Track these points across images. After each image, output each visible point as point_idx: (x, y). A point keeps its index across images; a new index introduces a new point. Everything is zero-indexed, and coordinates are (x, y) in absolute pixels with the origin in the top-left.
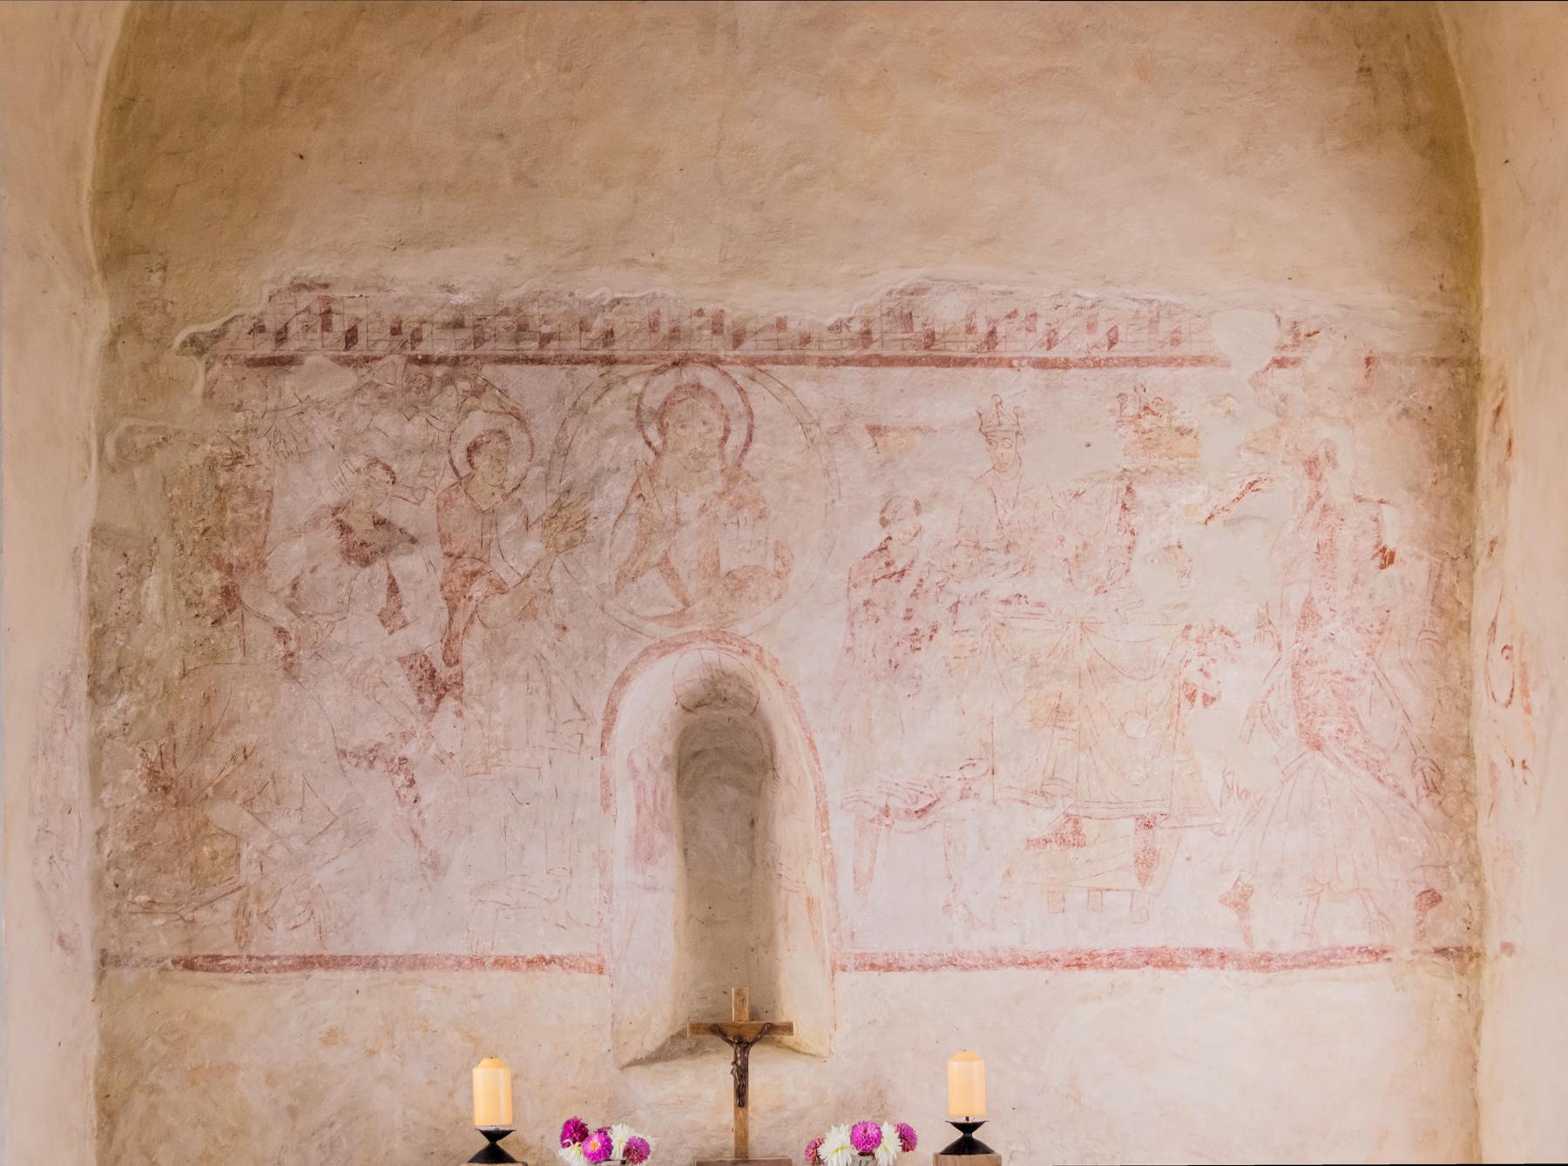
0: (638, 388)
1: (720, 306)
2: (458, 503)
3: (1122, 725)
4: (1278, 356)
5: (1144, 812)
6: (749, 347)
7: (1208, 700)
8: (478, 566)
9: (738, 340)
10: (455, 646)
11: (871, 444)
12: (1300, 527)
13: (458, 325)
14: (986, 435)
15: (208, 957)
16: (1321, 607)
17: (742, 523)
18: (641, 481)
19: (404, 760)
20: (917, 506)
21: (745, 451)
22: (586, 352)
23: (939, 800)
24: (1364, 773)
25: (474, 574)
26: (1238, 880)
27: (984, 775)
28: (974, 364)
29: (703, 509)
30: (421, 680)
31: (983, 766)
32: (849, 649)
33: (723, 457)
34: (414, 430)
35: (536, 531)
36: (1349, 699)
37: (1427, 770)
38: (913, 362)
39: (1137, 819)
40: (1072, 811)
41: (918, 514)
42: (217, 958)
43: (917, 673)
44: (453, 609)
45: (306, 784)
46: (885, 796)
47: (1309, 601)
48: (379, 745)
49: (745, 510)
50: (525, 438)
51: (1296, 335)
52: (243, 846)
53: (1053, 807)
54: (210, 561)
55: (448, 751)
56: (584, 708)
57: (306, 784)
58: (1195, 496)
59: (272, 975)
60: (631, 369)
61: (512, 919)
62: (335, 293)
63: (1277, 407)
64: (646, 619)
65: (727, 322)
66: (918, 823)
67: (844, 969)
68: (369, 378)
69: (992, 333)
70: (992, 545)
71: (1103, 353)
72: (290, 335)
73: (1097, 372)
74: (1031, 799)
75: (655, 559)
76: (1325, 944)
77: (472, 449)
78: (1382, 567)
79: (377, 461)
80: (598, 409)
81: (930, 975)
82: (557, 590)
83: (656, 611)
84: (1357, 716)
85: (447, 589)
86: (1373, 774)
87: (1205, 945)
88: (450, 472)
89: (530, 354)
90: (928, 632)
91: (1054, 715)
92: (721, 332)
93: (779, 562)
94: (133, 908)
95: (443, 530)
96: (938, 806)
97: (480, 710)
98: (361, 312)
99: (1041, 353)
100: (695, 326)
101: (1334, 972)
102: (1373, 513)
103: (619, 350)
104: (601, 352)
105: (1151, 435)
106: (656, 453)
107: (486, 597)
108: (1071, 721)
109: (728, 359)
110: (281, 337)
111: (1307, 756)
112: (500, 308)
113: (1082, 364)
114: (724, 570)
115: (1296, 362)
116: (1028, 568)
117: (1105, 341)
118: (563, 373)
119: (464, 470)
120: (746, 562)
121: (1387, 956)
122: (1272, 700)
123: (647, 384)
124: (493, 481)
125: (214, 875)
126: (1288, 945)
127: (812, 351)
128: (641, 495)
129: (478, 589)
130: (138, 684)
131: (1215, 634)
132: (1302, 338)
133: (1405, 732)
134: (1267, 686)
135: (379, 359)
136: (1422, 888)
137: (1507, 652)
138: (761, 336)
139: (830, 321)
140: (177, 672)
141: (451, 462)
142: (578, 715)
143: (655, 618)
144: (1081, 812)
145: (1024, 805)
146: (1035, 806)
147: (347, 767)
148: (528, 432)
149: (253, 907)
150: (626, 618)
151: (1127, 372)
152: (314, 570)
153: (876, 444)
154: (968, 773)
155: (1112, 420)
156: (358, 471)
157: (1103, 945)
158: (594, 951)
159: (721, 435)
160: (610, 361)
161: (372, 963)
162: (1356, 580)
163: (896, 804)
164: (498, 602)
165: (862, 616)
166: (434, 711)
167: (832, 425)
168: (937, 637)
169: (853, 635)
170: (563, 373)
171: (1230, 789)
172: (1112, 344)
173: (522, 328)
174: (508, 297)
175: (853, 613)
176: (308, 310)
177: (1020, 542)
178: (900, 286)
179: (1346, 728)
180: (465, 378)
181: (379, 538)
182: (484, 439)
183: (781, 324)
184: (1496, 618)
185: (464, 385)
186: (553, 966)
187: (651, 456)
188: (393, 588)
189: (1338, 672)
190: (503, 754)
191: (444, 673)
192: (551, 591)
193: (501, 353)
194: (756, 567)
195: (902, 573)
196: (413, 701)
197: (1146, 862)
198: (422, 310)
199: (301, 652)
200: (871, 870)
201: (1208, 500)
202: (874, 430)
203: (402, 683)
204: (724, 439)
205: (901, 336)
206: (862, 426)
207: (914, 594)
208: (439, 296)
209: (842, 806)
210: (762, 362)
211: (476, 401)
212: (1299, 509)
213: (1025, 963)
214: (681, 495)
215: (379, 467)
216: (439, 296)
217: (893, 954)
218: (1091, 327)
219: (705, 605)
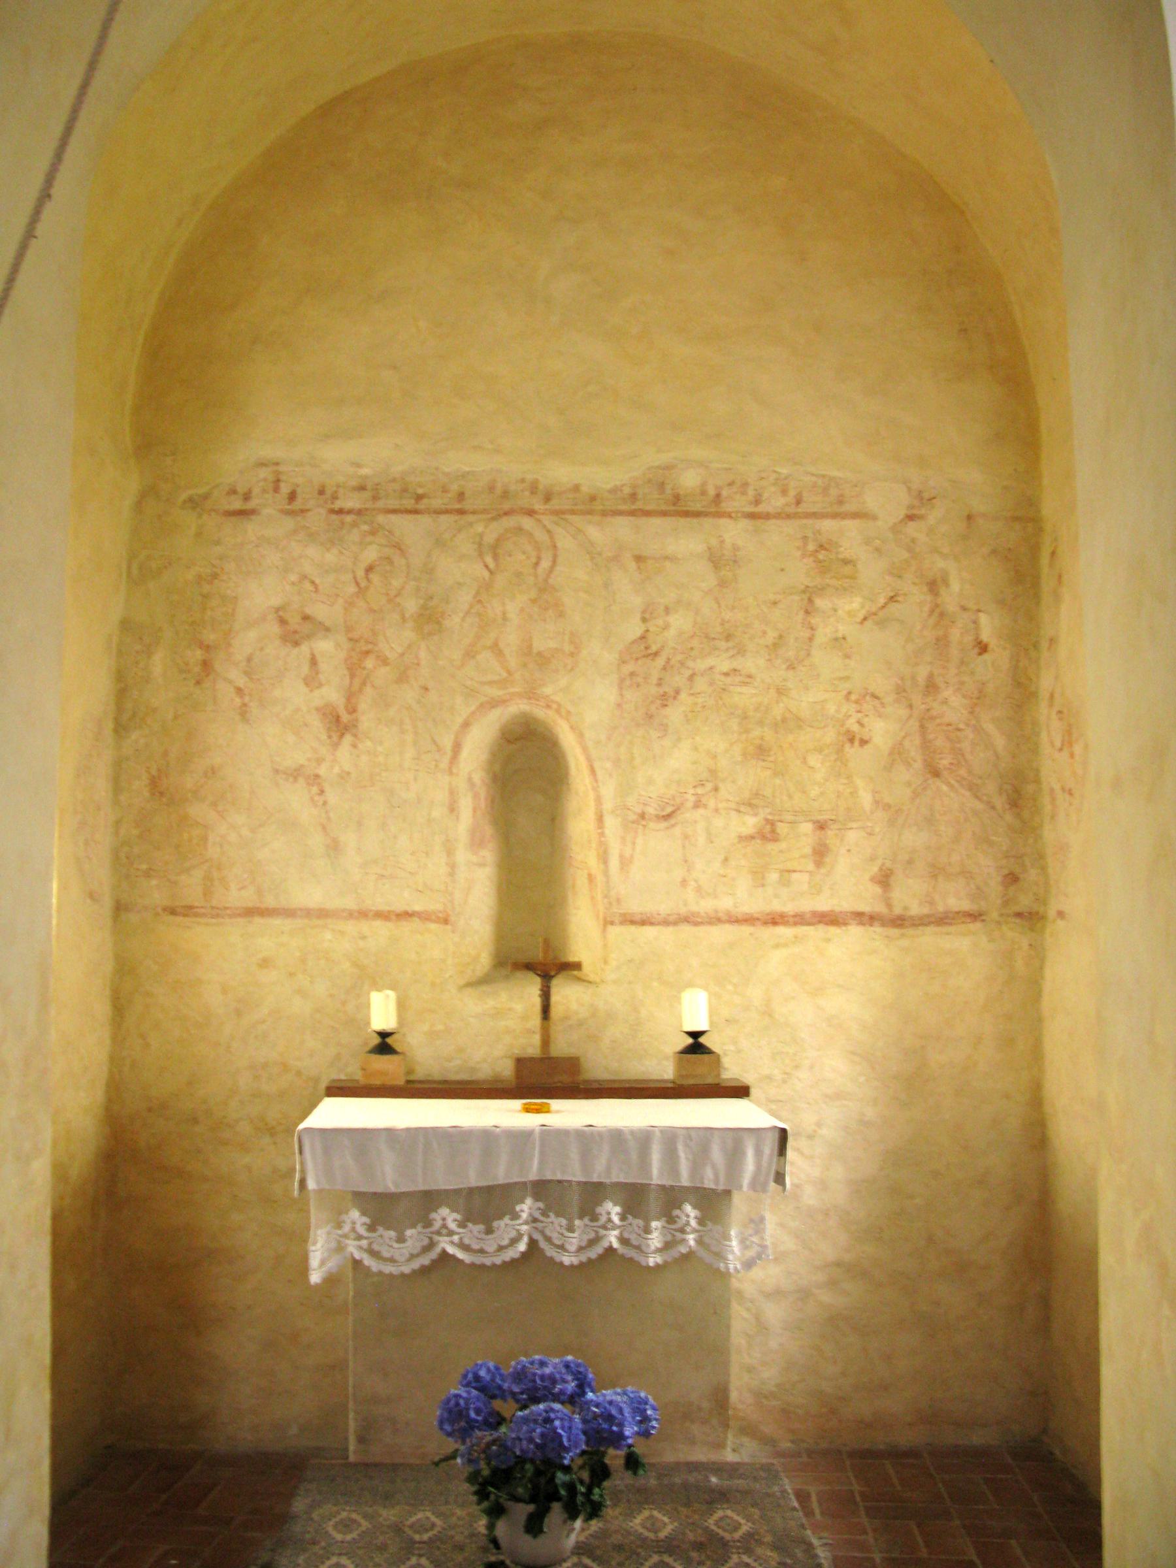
33: (536, 576)
35: (410, 624)
38: (664, 514)
50: (403, 561)
83: (489, 678)
89: (409, 507)
103: (467, 505)
109: (541, 511)
114: (535, 651)
127: (598, 506)
150: (469, 683)
160: (461, 512)
165: (628, 682)
187: (486, 574)
192: (418, 664)
193: (391, 507)
194: (556, 649)
195: (656, 654)
204: (537, 564)
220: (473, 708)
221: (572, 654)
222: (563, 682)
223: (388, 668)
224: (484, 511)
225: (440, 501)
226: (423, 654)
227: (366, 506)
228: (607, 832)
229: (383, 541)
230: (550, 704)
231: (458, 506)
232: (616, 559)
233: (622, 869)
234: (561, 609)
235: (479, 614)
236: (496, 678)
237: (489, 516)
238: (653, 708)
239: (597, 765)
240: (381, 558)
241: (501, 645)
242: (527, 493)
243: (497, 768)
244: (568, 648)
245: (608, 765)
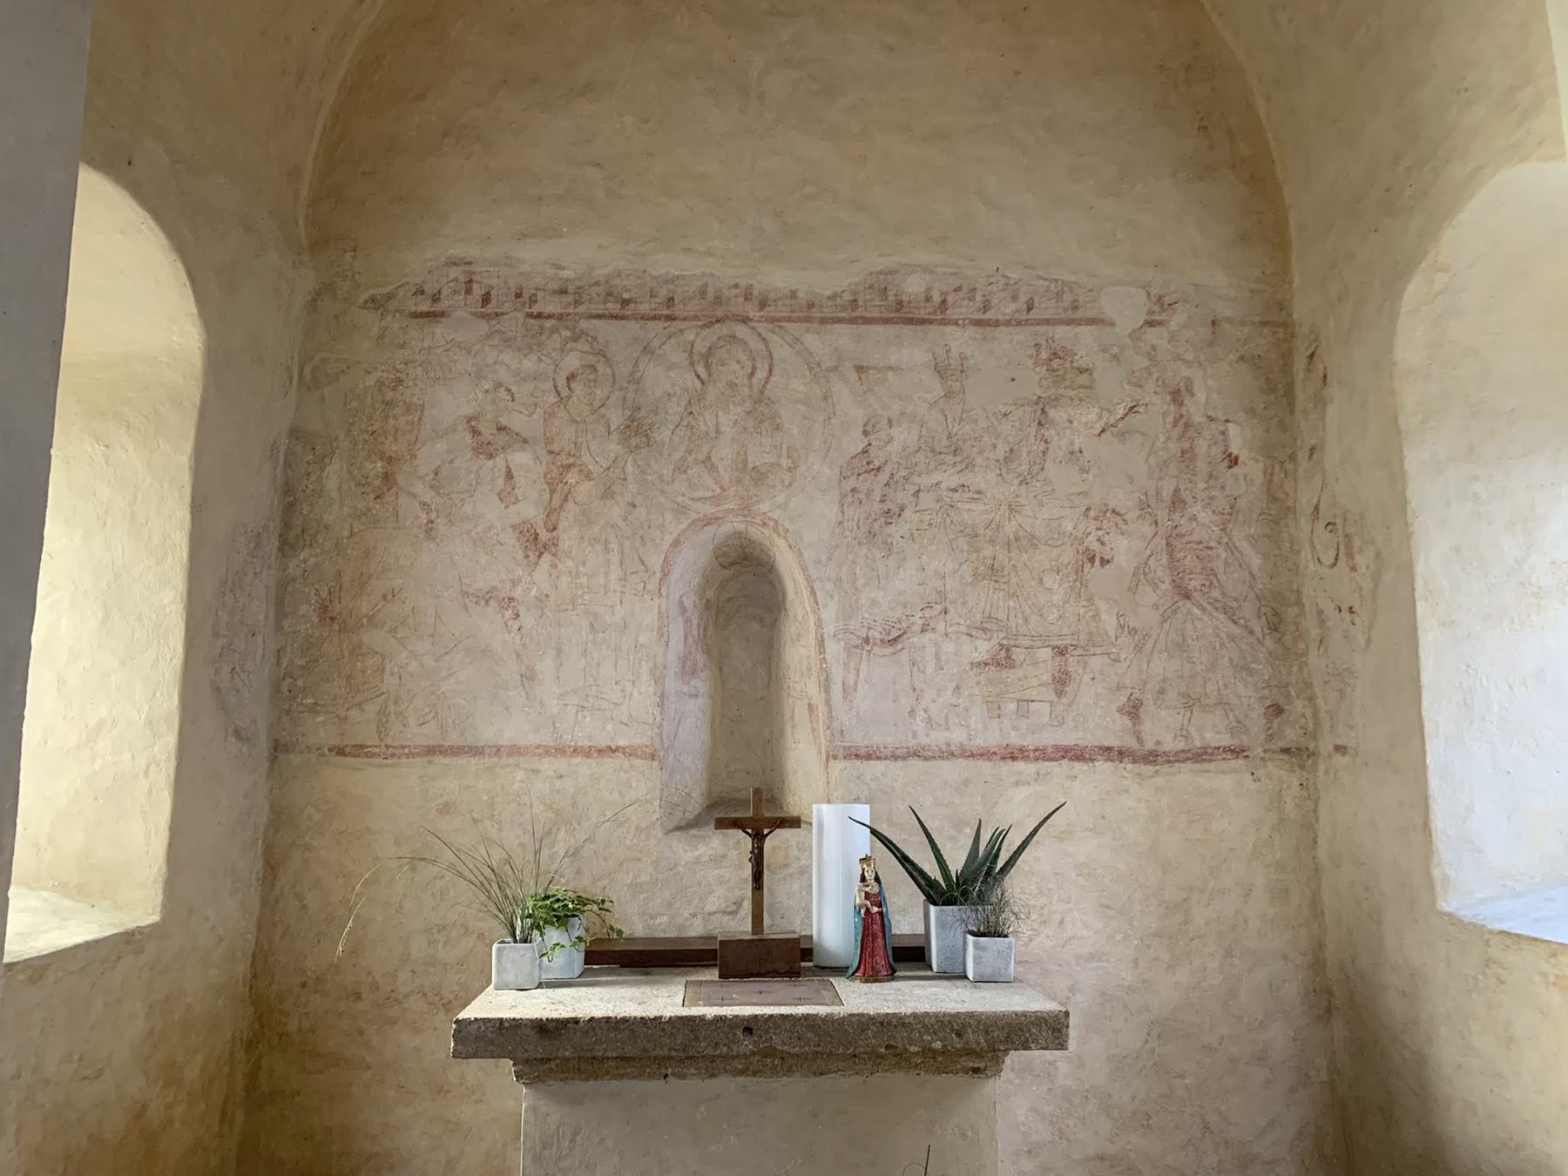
0: (691, 337)
1: (750, 282)
2: (559, 415)
3: (1041, 579)
4: (1149, 318)
5: (1059, 643)
6: (770, 311)
7: (1104, 562)
8: (572, 460)
9: (763, 305)
10: (554, 517)
12: (1168, 439)
13: (564, 292)
14: (939, 372)
15: (356, 746)
16: (1186, 495)
17: (764, 433)
19: (511, 599)
20: (890, 421)
21: (766, 382)
23: (905, 633)
24: (1222, 617)
25: (569, 466)
26: (1131, 695)
27: (940, 614)
28: (931, 323)
29: (736, 422)
30: (528, 541)
31: (938, 608)
33: (751, 386)
34: (529, 364)
35: (615, 436)
36: (1209, 562)
37: (1268, 615)
38: (886, 321)
39: (1053, 649)
40: (1005, 642)
41: (891, 427)
42: (362, 747)
43: (889, 541)
44: (552, 492)
45: (438, 616)
47: (1177, 491)
48: (494, 588)
50: (609, 371)
51: (1162, 304)
52: (387, 661)
53: (990, 639)
54: (375, 454)
55: (545, 592)
57: (438, 616)
58: (1089, 416)
59: (404, 760)
60: (686, 324)
61: (588, 719)
62: (476, 268)
63: (1149, 354)
65: (756, 293)
66: (890, 650)
67: (835, 758)
68: (498, 326)
69: (944, 302)
70: (943, 450)
71: (1024, 316)
72: (442, 297)
73: (1018, 329)
74: (974, 633)
75: (701, 458)
76: (1199, 745)
77: (571, 378)
78: (1230, 467)
79: (501, 385)
80: (662, 352)
81: (900, 763)
82: (629, 478)
84: (1215, 575)
85: (549, 476)
86: (1229, 618)
87: (1107, 744)
88: (553, 393)
90: (897, 510)
91: (989, 572)
92: (751, 299)
93: (790, 461)
94: (302, 708)
95: (548, 434)
96: (905, 636)
97: (570, 563)
98: (494, 282)
99: (979, 316)
100: (732, 295)
101: (1206, 766)
102: (1222, 428)
103: (678, 311)
104: (665, 312)
105: (1061, 372)
108: (1003, 576)
110: (436, 298)
111: (1180, 604)
112: (593, 281)
113: (1008, 323)
114: (751, 465)
115: (1161, 323)
116: (969, 466)
117: (1025, 307)
118: (638, 326)
119: (565, 392)
121: (1245, 754)
122: (1152, 562)
123: (697, 334)
124: (585, 401)
125: (364, 684)
126: (1170, 744)
127: (816, 314)
128: (691, 413)
129: (572, 477)
130: (316, 542)
131: (1108, 514)
132: (1166, 307)
133: (1251, 587)
134: (1149, 552)
135: (506, 314)
136: (1269, 703)
137: (1330, 527)
138: (780, 303)
139: (828, 293)
140: (346, 533)
141: (555, 387)
142: (642, 568)
144: (1012, 643)
145: (969, 638)
146: (977, 638)
147: (469, 604)
148: (611, 367)
149: (392, 708)
150: (679, 499)
151: (1042, 329)
152: (451, 462)
153: (860, 379)
154: (928, 613)
155: (1030, 363)
156: (487, 391)
157: (1030, 742)
158: (649, 743)
159: (750, 371)
161: (477, 751)
162: (1211, 476)
163: (875, 634)
164: (586, 486)
166: (536, 564)
168: (903, 515)
170: (638, 326)
171: (1122, 627)
172: (1029, 309)
173: (609, 294)
174: (600, 273)
175: (844, 496)
176: (456, 280)
177: (964, 448)
178: (878, 269)
179: (1207, 583)
180: (567, 328)
181: (501, 439)
183: (793, 294)
184: (1319, 502)
185: (568, 333)
186: (617, 754)
187: (698, 384)
188: (509, 476)
189: (1201, 542)
191: (544, 536)
192: (625, 479)
193: (594, 312)
194: (772, 464)
195: (879, 469)
196: (520, 555)
197: (1061, 682)
198: (539, 281)
199: (439, 520)
200: (856, 683)
201: (1100, 417)
202: (860, 369)
203: (509, 538)
204: (752, 374)
205: (878, 303)
207: (887, 484)
208: (551, 272)
209: (834, 636)
210: (779, 320)
211: (574, 345)
212: (1168, 426)
213: (972, 755)
214: (720, 413)
215: (502, 389)
216: (551, 272)
217: (872, 746)
218: (1014, 298)
220: (683, 526)
224: (696, 318)
232: (835, 369)
245: (829, 586)
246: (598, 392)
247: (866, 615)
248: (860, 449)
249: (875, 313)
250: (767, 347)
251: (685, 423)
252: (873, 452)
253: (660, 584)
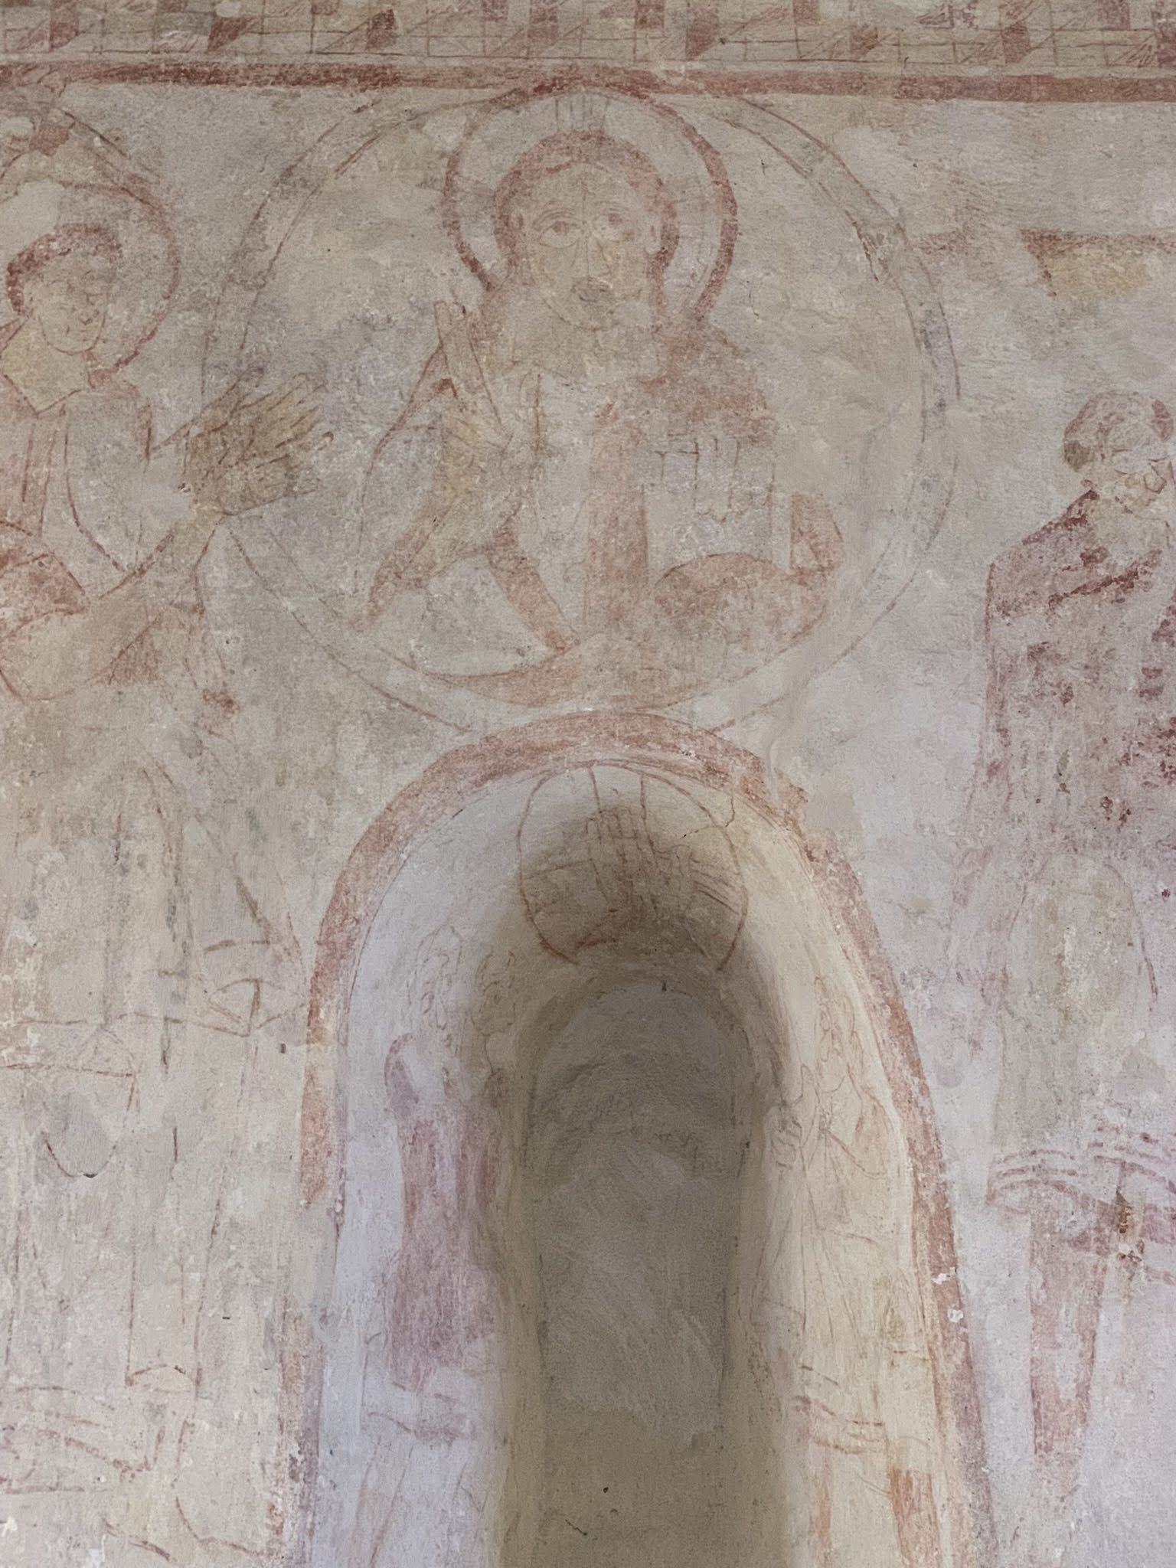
0: (450, 140)
11: (1035, 276)
17: (707, 451)
18: (450, 348)
22: (323, 59)
32: (993, 769)
33: (658, 299)
35: (169, 459)
38: (1128, 91)
46: (1116, 1171)
49: (716, 419)
50: (157, 244)
56: (267, 912)
60: (431, 97)
64: (448, 680)
75: (476, 535)
83: (477, 661)
89: (187, 59)
92: (659, 22)
103: (404, 55)
106: (489, 287)
107: (25, 621)
109: (675, 81)
114: (657, 562)
120: (716, 545)
123: (472, 129)
124: (71, 343)
127: (884, 65)
128: (446, 383)
138: (757, 33)
143: (471, 680)
148: (167, 232)
150: (395, 678)
153: (1048, 275)
159: (654, 247)
160: (379, 78)
165: (1025, 683)
167: (937, 229)
169: (1003, 731)
175: (1002, 675)
182: (55, 245)
187: (471, 290)
190: (33, 1038)
192: (199, 609)
193: (117, 59)
194: (740, 557)
195: (1128, 580)
200: (1083, 1391)
204: (663, 257)
205: (1099, 37)
206: (1009, 232)
209: (991, 1197)
210: (757, 86)
211: (43, 162)
214: (549, 384)
219: (607, 650)
220: (409, 775)
221: (801, 576)
222: (771, 678)
223: (76, 620)
224: (466, 77)
225: (301, 42)
226: (217, 574)
227: (29, 57)
228: (970, 1281)
229: (85, 172)
230: (719, 760)
231: (363, 59)
232: (956, 243)
233: (1043, 1449)
234: (758, 413)
235: (439, 433)
236: (508, 662)
237: (489, 93)
238: (1130, 781)
239: (916, 1000)
240: (70, 231)
241: (525, 541)
242: (624, 23)
243: (505, 1050)
244: (784, 553)
245: (963, 1001)
246: (117, 313)
247: (1113, 1117)
248: (1057, 511)
249: (1093, 68)
250: (716, 169)
251: (422, 418)
252: (1103, 522)
253: (314, 990)
